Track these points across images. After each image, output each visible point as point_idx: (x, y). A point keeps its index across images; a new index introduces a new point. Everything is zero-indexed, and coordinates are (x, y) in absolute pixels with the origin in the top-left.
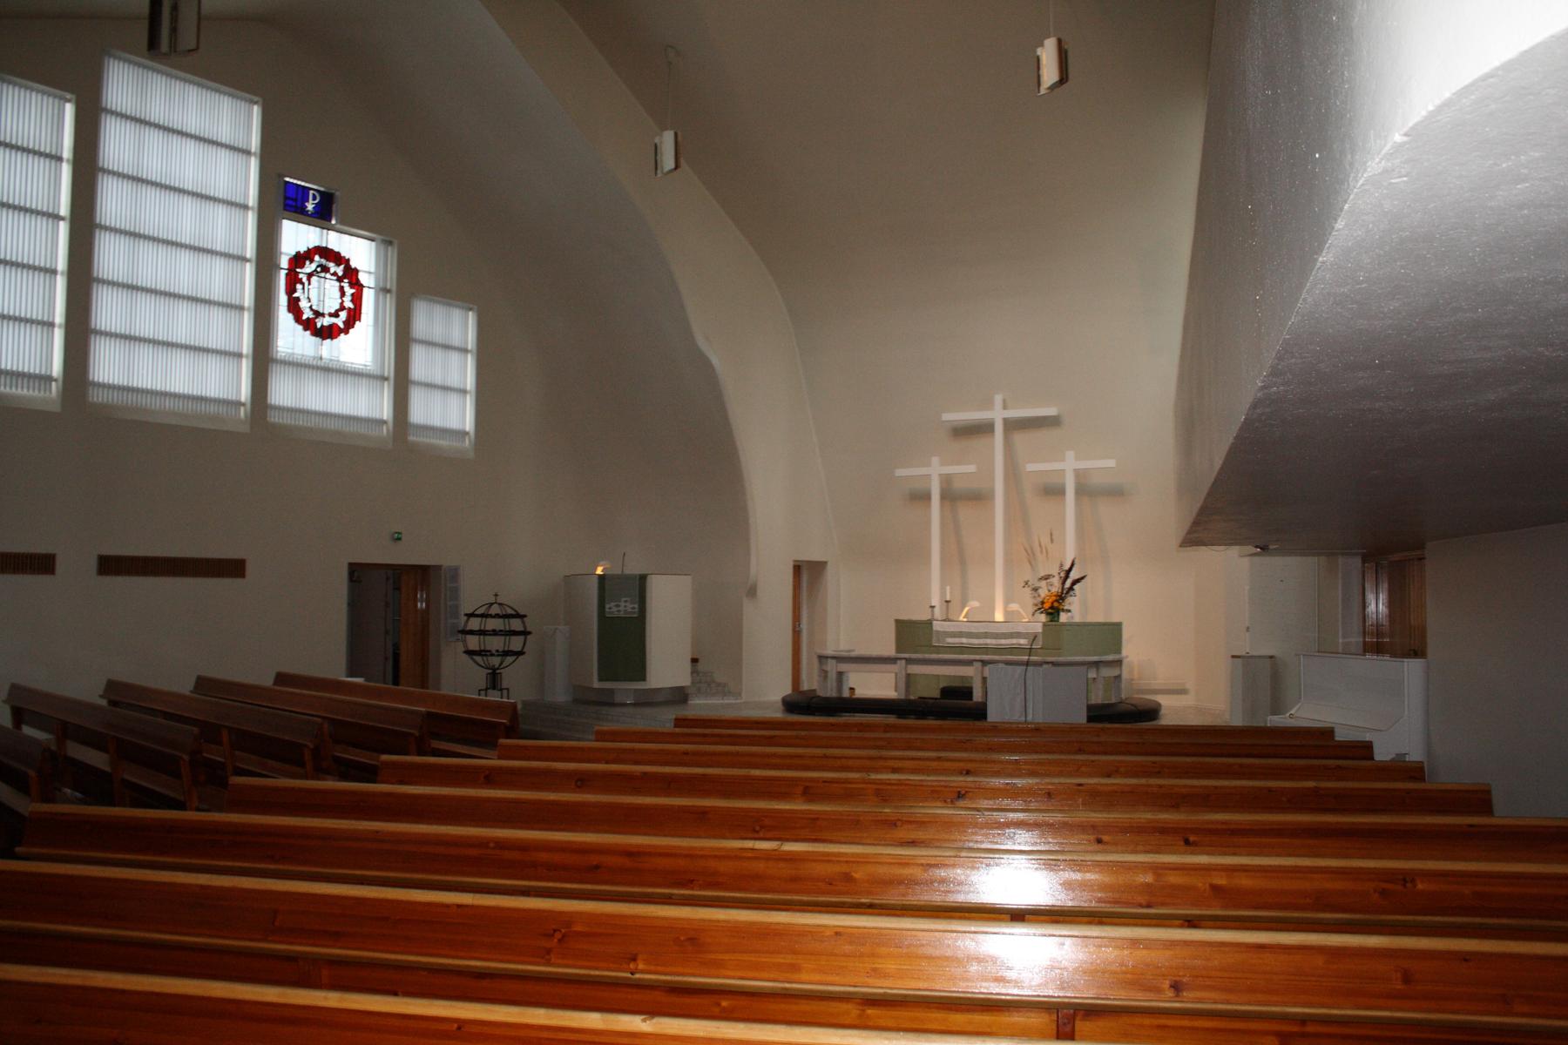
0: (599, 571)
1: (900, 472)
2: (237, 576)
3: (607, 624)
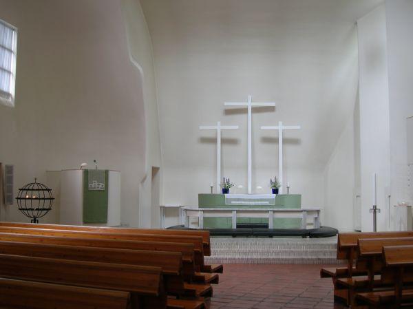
0: (83, 164)
1: (201, 128)
2: (202, 195)
3: (87, 191)
